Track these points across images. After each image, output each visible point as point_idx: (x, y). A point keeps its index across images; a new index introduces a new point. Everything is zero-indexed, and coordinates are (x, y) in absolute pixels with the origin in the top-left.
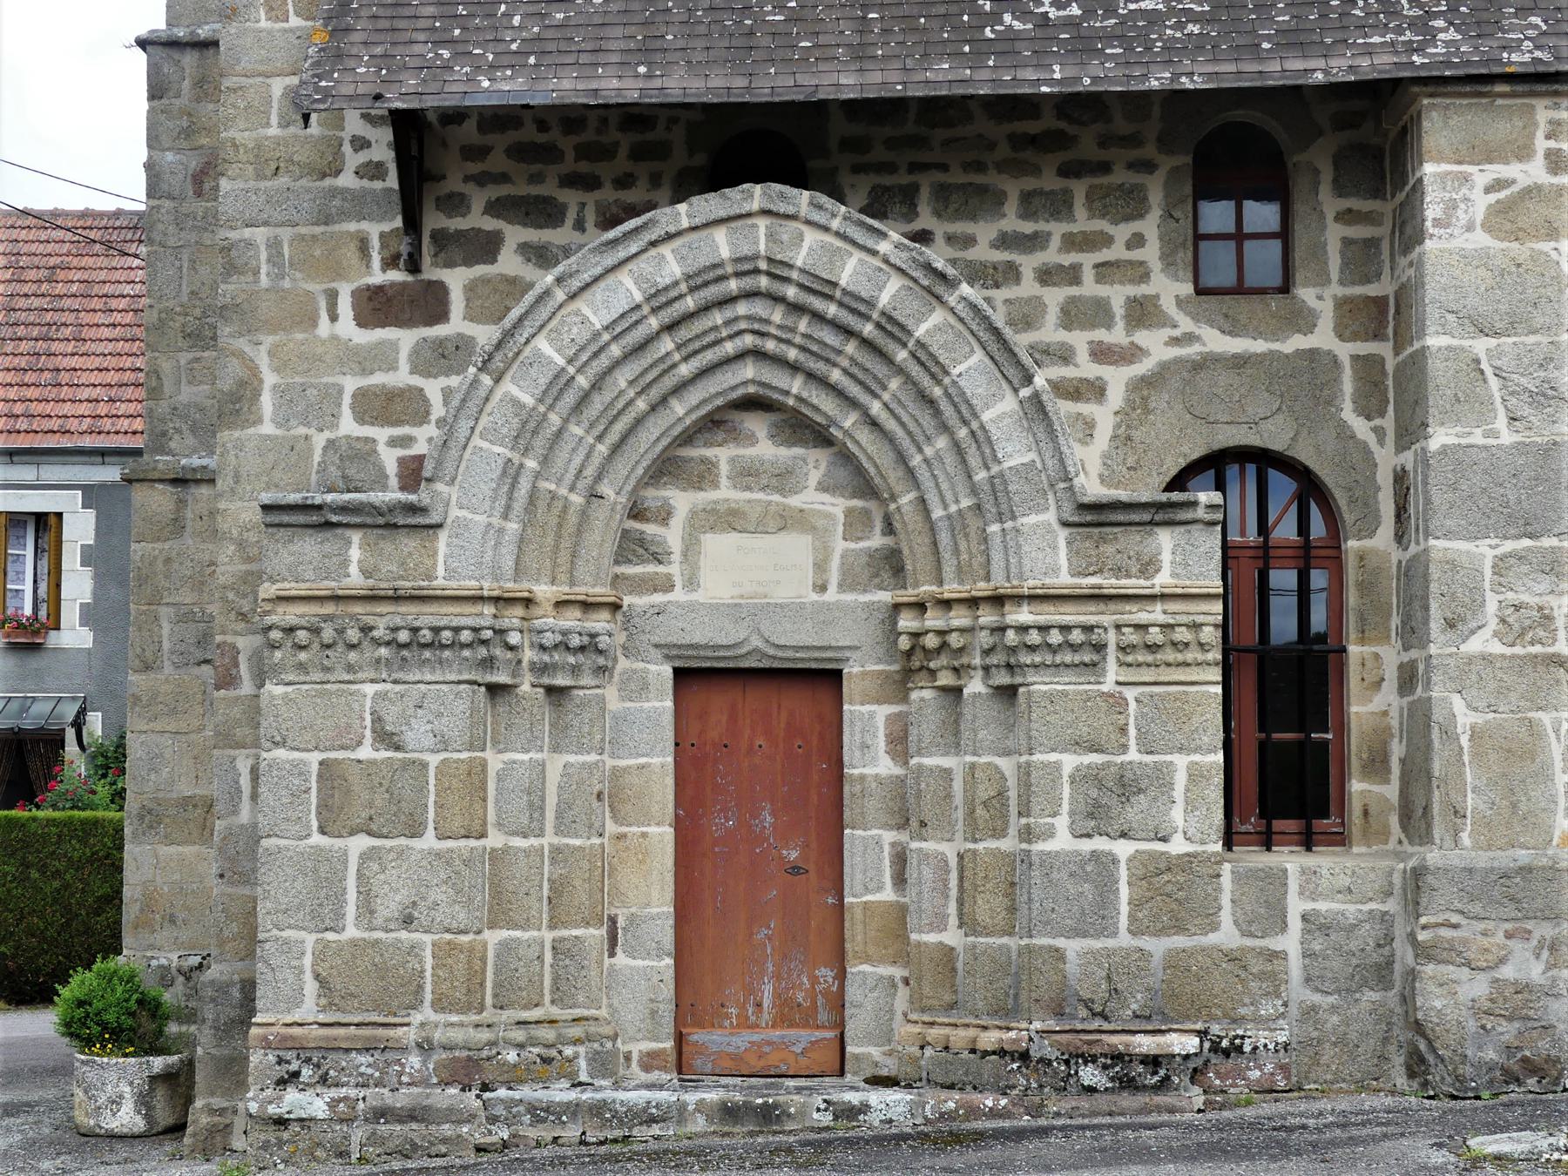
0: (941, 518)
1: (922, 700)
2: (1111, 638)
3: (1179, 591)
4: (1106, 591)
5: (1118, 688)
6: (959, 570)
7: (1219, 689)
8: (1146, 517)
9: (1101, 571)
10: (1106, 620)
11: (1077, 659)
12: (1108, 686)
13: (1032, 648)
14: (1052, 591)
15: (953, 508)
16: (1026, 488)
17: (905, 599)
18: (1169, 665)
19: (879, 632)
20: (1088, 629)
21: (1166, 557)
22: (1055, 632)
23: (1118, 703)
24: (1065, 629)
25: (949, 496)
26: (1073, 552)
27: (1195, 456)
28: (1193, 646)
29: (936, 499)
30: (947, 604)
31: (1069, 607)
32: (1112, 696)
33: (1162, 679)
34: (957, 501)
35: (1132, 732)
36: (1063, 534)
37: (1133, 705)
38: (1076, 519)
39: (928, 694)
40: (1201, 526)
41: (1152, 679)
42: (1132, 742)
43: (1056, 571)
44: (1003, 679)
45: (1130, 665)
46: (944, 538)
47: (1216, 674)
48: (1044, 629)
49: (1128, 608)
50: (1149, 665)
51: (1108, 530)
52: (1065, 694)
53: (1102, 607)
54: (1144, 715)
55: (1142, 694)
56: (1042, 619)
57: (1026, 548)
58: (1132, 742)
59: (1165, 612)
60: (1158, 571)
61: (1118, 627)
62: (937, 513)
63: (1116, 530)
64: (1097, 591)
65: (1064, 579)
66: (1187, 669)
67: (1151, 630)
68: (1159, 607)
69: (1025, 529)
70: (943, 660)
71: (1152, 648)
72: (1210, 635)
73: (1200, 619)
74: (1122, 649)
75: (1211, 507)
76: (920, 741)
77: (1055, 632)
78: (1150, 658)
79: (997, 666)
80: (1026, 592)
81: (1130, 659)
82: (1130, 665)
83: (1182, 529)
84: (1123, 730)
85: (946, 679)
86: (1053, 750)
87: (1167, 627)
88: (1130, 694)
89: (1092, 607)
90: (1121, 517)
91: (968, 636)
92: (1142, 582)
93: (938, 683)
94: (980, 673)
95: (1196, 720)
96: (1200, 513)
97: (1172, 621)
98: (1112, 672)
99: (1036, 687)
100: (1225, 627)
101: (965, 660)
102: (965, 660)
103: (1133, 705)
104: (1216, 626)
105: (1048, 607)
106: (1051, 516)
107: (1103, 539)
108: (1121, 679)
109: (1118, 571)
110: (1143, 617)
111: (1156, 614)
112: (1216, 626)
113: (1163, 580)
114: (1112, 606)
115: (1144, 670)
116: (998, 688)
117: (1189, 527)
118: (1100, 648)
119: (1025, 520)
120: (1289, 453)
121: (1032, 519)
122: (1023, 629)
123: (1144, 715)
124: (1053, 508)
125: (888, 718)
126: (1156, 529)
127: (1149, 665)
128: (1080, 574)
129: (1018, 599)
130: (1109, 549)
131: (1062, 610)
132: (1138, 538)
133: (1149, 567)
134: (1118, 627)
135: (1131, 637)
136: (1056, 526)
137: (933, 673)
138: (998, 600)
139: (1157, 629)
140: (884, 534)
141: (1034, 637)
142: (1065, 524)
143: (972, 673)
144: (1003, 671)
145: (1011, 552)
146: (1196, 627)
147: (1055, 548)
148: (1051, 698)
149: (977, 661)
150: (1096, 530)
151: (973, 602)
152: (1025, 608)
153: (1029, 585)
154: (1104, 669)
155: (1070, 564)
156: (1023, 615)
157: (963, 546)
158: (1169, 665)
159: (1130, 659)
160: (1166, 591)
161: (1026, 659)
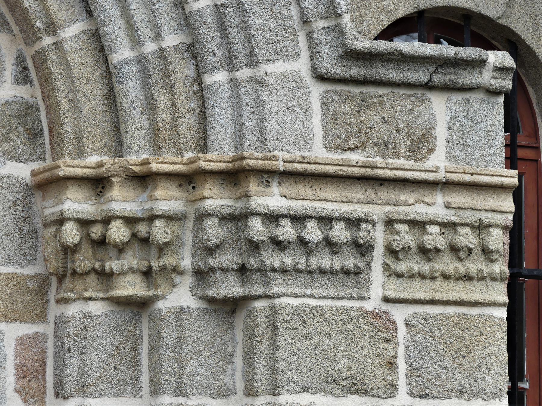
0: (128, 61)
1: (87, 316)
2: (380, 237)
3: (468, 178)
4: (380, 173)
5: (385, 307)
6: (155, 134)
7: (502, 313)
8: (423, 77)
9: (363, 146)
10: (377, 212)
11: (338, 264)
12: (373, 304)
13: (279, 245)
14: (313, 168)
15: (150, 47)
16: (271, 23)
17: (78, 172)
18: (446, 277)
19: (9, 219)
20: (354, 223)
21: (441, 133)
22: (312, 224)
23: (382, 324)
24: (326, 221)
25: (144, 30)
26: (330, 118)
27: (400, 14)
28: (477, 254)
29: (123, 33)
30: (143, 179)
31: (329, 191)
32: (378, 316)
33: (439, 296)
34: (158, 37)
35: (402, 367)
36: (317, 91)
37: (402, 330)
38: (338, 71)
39: (97, 308)
40: (480, 95)
41: (428, 296)
42: (402, 382)
43: (306, 139)
44: (231, 288)
45: (399, 275)
46: (131, 90)
47: (500, 293)
48: (298, 219)
49: (403, 197)
50: (423, 277)
51: (371, 90)
52: (320, 311)
53: (370, 194)
54: (417, 345)
55: (414, 316)
56: (298, 206)
57: (271, 107)
58: (402, 382)
59: (447, 206)
60: (431, 151)
61: (389, 223)
62: (122, 53)
63: (381, 91)
64: (368, 172)
65: (319, 153)
66: (468, 285)
67: (461, 230)
68: (439, 198)
69: (270, 81)
70: (131, 260)
71: (426, 253)
72: (498, 240)
73: (488, 218)
74: (392, 252)
75: (501, 70)
76: (82, 374)
77: (312, 224)
78: (426, 268)
79: (223, 270)
80: (281, 166)
81: (402, 267)
82: (399, 275)
83: (458, 97)
84: (391, 364)
85: (131, 287)
86: (305, 390)
87: (448, 226)
88: (399, 314)
89: (358, 193)
90: (392, 73)
91: (175, 226)
92: (411, 164)
93: (119, 292)
94: (188, 280)
95: (478, 353)
96: (486, 77)
97: (455, 219)
98: (378, 284)
99: (284, 300)
100: (515, 232)
101: (168, 260)
102: (168, 260)
103: (402, 330)
104: (504, 228)
105: (304, 189)
106: (302, 65)
107: (365, 104)
108: (391, 294)
109: (384, 147)
110: (420, 211)
111: (435, 207)
112: (504, 228)
113: (438, 163)
114: (384, 194)
115: (417, 283)
116: (211, 301)
117: (467, 95)
118: (363, 249)
119: (270, 68)
120: (503, 22)
121: (278, 68)
122: (272, 218)
123: (417, 345)
124: (305, 54)
125: (20, 341)
126: (431, 95)
127: (423, 277)
128: (337, 148)
129: (267, 175)
130: (373, 117)
131: (323, 194)
132: (408, 104)
133: (421, 144)
134: (389, 223)
135: (406, 237)
136: (308, 79)
137: (106, 277)
138: (234, 176)
139: (467, 230)
140: (17, 82)
141: (287, 231)
142: (322, 78)
143: (177, 279)
144: (232, 277)
145: (246, 112)
146: (481, 228)
147: (307, 109)
148: (302, 315)
149: (187, 263)
150: (356, 90)
151: (189, 179)
152: (275, 189)
153: (282, 158)
154: (368, 281)
155: (326, 133)
156: (272, 198)
157: (162, 100)
158: (446, 277)
159: (402, 267)
160: (454, 177)
161: (272, 259)
